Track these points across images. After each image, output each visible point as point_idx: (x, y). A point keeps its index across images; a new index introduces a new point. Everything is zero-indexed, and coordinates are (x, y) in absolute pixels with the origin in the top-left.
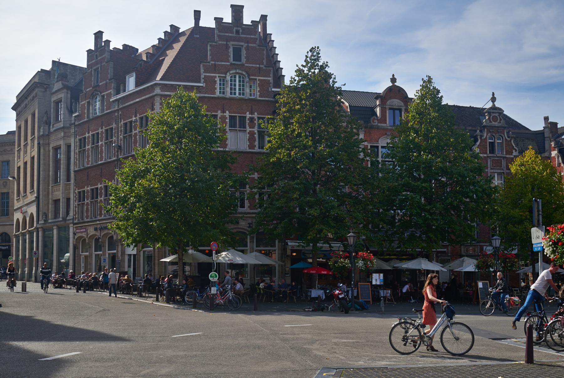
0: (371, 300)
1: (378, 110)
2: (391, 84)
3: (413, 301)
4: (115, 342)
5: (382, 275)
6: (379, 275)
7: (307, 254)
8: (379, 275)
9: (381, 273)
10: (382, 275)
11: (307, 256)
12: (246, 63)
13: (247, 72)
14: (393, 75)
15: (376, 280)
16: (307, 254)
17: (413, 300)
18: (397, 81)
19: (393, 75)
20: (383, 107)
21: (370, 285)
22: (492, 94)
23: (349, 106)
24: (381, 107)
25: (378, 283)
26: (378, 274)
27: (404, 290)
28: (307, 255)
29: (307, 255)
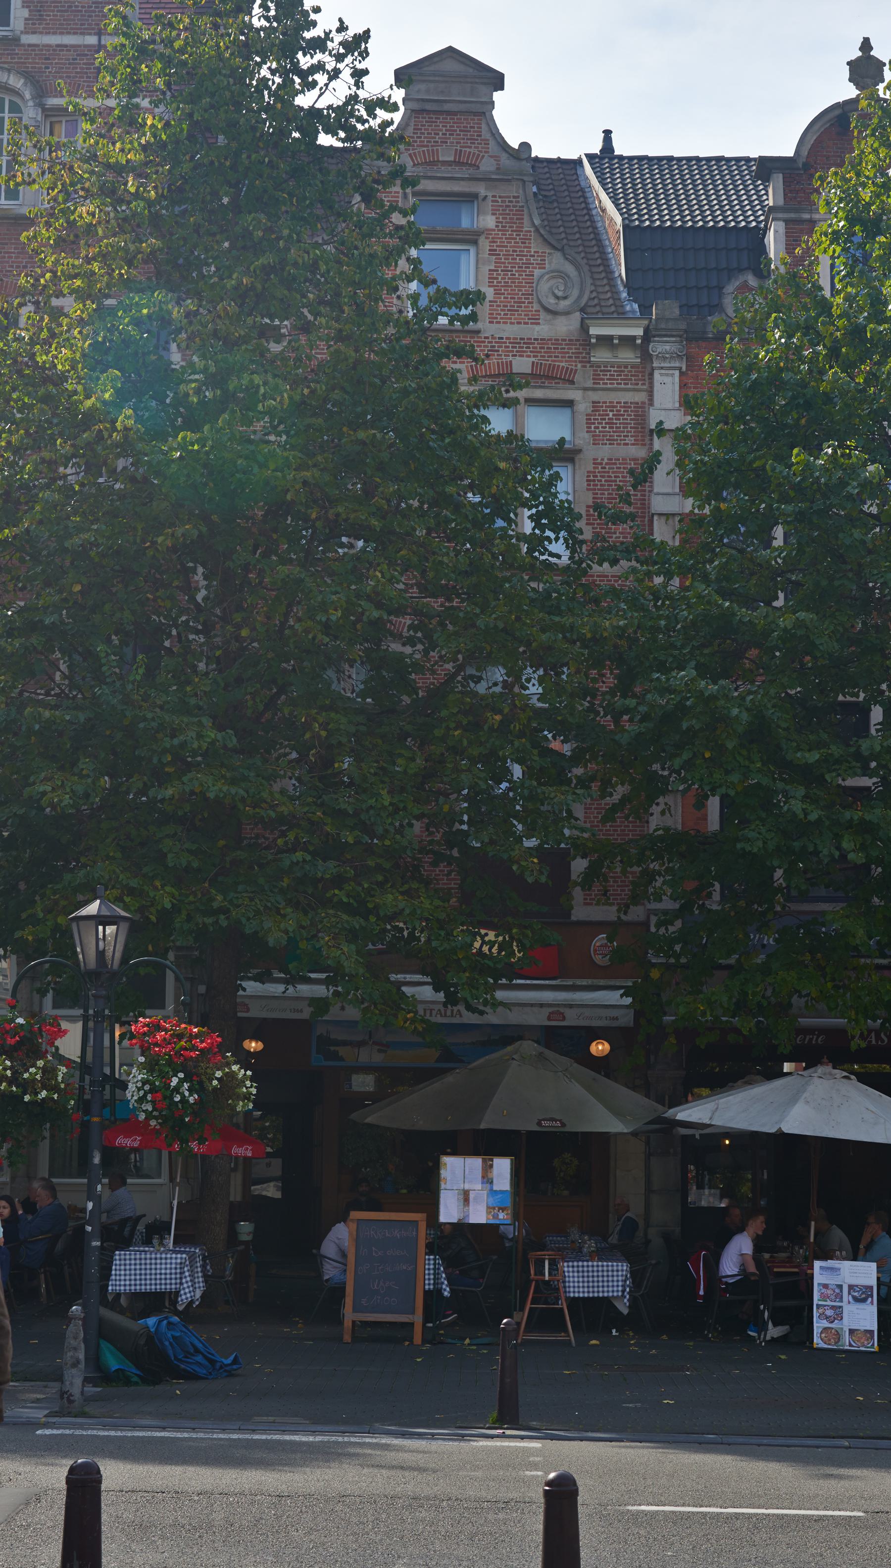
0: (418, 1318)
1: (773, 242)
2: (850, 92)
3: (773, 1332)
4: (780, 1461)
5: (503, 1166)
6: (487, 1168)
7: (344, 1043)
8: (487, 1168)
9: (502, 1154)
10: (503, 1166)
11: (342, 1059)
12: (26, 32)
13: (28, 76)
14: (866, 45)
15: (465, 1197)
16: (344, 1043)
17: (775, 1325)
18: (846, 71)
19: (866, 45)
20: (801, 221)
21: (423, 1226)
22: (360, 31)
23: (625, 227)
24: (787, 221)
25: (478, 1215)
26: (476, 1163)
27: (729, 1266)
28: (342, 1051)
29: (342, 1051)
